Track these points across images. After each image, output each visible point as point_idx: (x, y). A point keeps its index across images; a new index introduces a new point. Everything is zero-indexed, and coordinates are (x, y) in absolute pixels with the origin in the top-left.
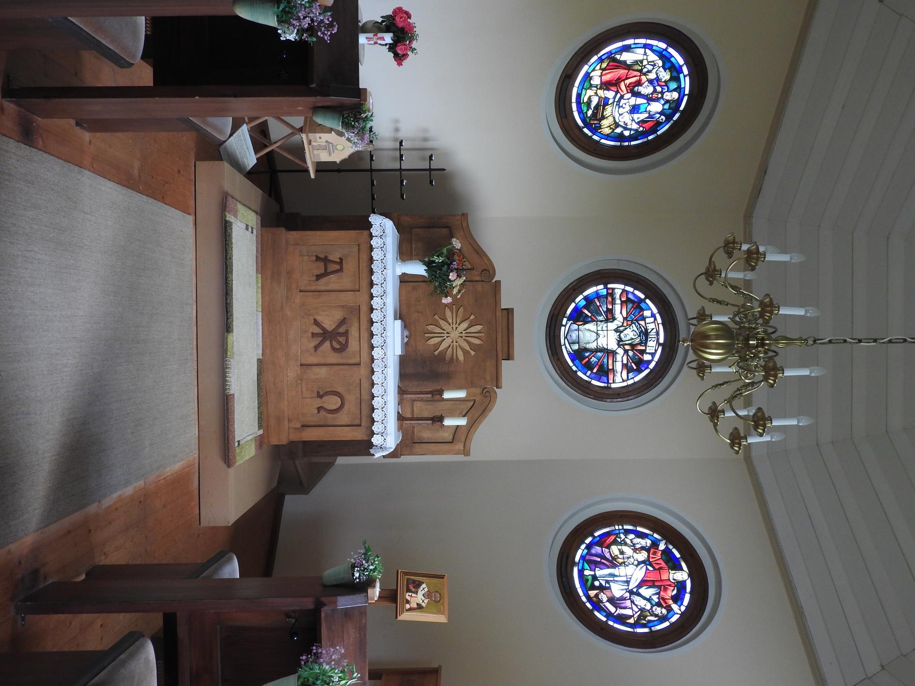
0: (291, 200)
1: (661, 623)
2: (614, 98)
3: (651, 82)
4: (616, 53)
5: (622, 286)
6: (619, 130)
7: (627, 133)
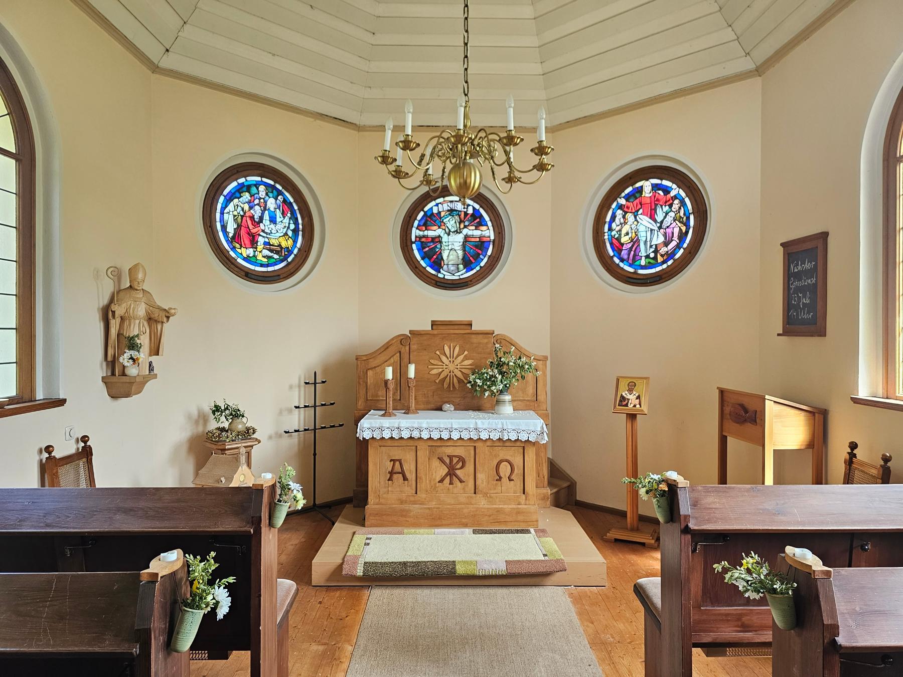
0: (341, 491)
3: (251, 208)
4: (228, 237)
5: (414, 229)
6: (290, 233)
7: (292, 227)
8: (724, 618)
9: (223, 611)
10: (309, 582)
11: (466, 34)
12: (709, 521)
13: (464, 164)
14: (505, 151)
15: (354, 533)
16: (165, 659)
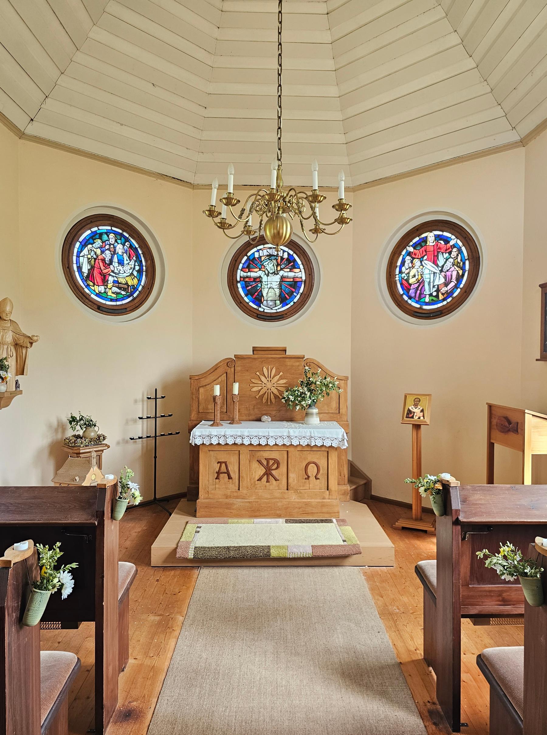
1: (462, 252)
2: (113, 276)
3: (102, 252)
5: (239, 271)
6: (135, 273)
7: (137, 268)
8: (488, 594)
9: (67, 592)
10: (148, 563)
11: (279, 109)
12: (475, 515)
13: (277, 217)
14: (311, 207)
15: (187, 523)
16: (18, 632)
